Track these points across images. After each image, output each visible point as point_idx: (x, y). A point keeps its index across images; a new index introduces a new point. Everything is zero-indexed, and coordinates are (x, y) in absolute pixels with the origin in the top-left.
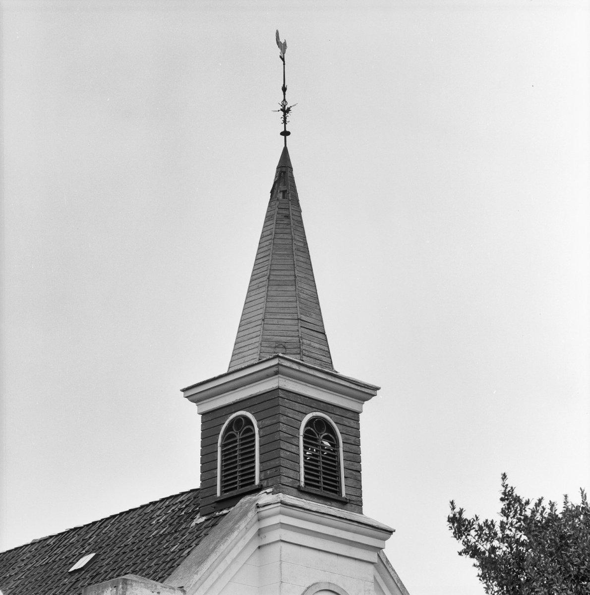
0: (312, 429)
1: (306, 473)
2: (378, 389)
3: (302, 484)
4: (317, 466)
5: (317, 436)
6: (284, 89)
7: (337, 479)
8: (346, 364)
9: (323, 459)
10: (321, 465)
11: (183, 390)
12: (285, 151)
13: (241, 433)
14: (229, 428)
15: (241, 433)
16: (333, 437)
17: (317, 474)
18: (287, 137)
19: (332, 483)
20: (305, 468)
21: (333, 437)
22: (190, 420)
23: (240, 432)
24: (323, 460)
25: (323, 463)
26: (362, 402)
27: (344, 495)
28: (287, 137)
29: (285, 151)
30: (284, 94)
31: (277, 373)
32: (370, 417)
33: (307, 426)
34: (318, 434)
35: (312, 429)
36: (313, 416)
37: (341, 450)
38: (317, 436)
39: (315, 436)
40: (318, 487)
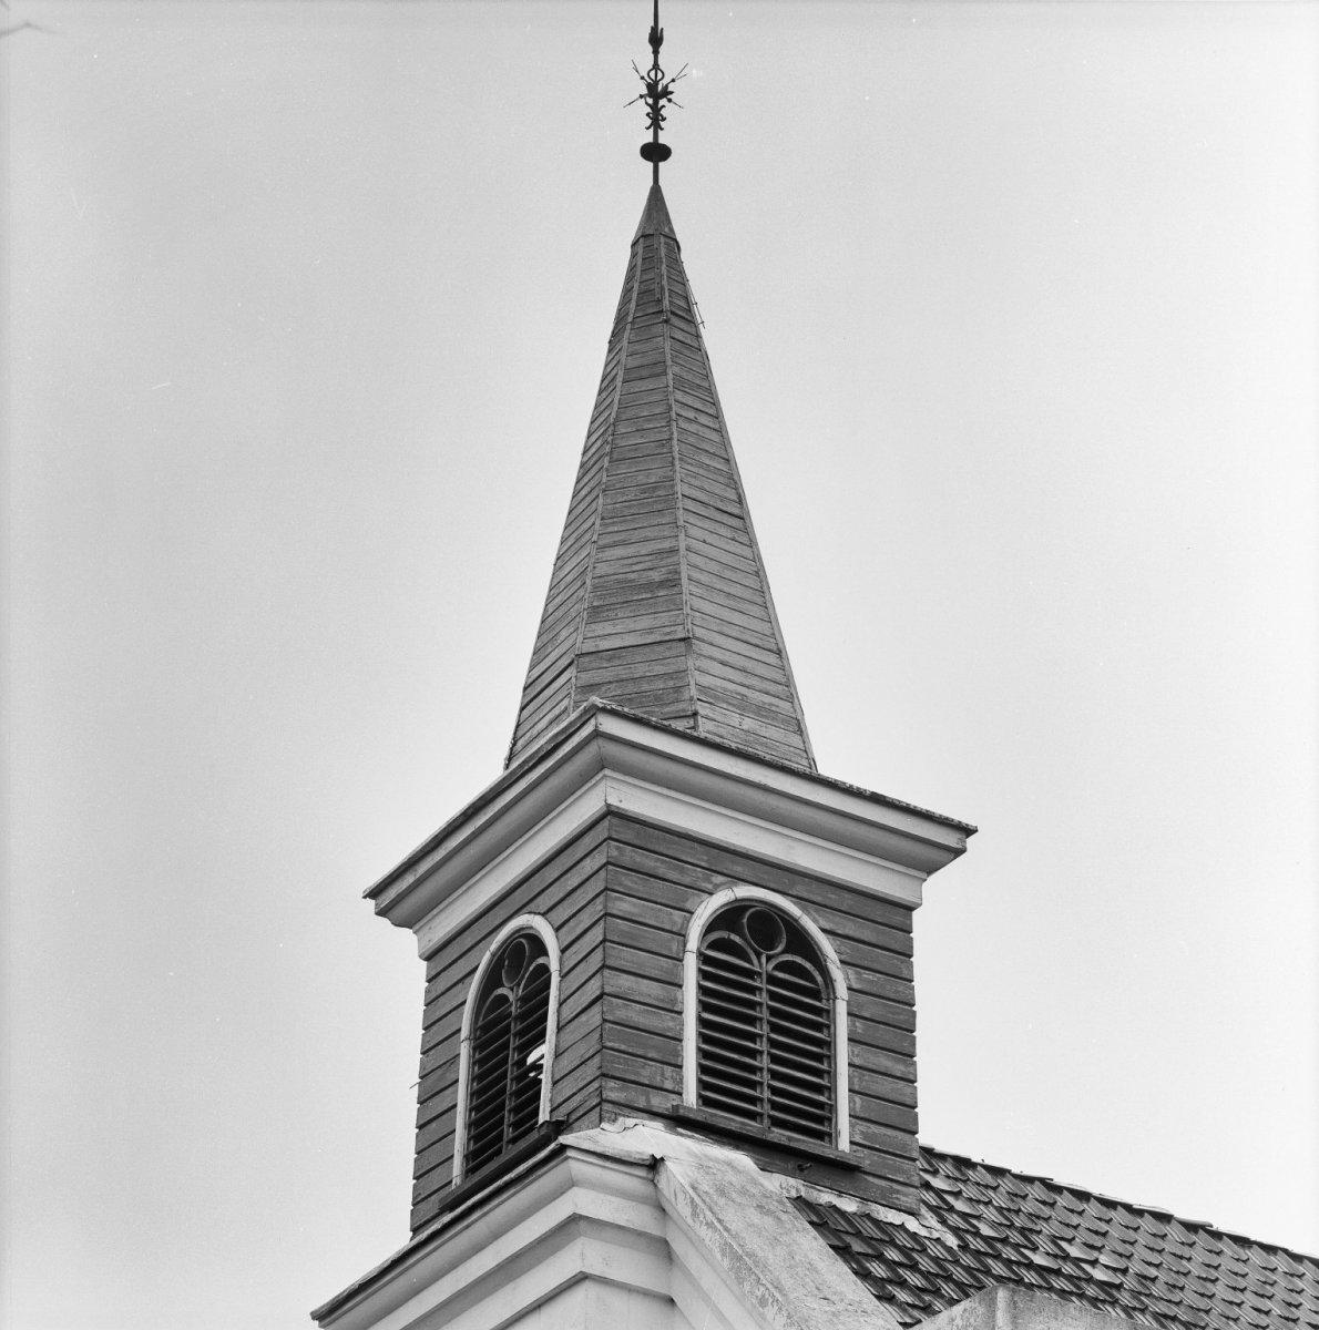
0: (737, 939)
1: (703, 1069)
2: (968, 831)
3: (690, 1097)
4: (753, 1100)
5: (755, 961)
6: (656, 39)
7: (825, 1067)
8: (852, 741)
9: (773, 1108)
10: (767, 1094)
11: (374, 894)
12: (656, 198)
13: (521, 987)
14: (492, 980)
15: (521, 987)
16: (808, 965)
17: (752, 1045)
18: (661, 164)
19: (806, 1093)
20: (702, 1022)
21: (808, 965)
22: (397, 968)
23: (519, 985)
24: (771, 1003)
25: (773, 996)
26: (923, 875)
27: (844, 1144)
28: (661, 164)
29: (656, 198)
30: (656, 53)
31: (601, 764)
32: (943, 914)
33: (711, 928)
34: (758, 955)
35: (737, 939)
36: (736, 900)
37: (841, 1009)
38: (755, 961)
39: (749, 961)
40: (752, 1116)
